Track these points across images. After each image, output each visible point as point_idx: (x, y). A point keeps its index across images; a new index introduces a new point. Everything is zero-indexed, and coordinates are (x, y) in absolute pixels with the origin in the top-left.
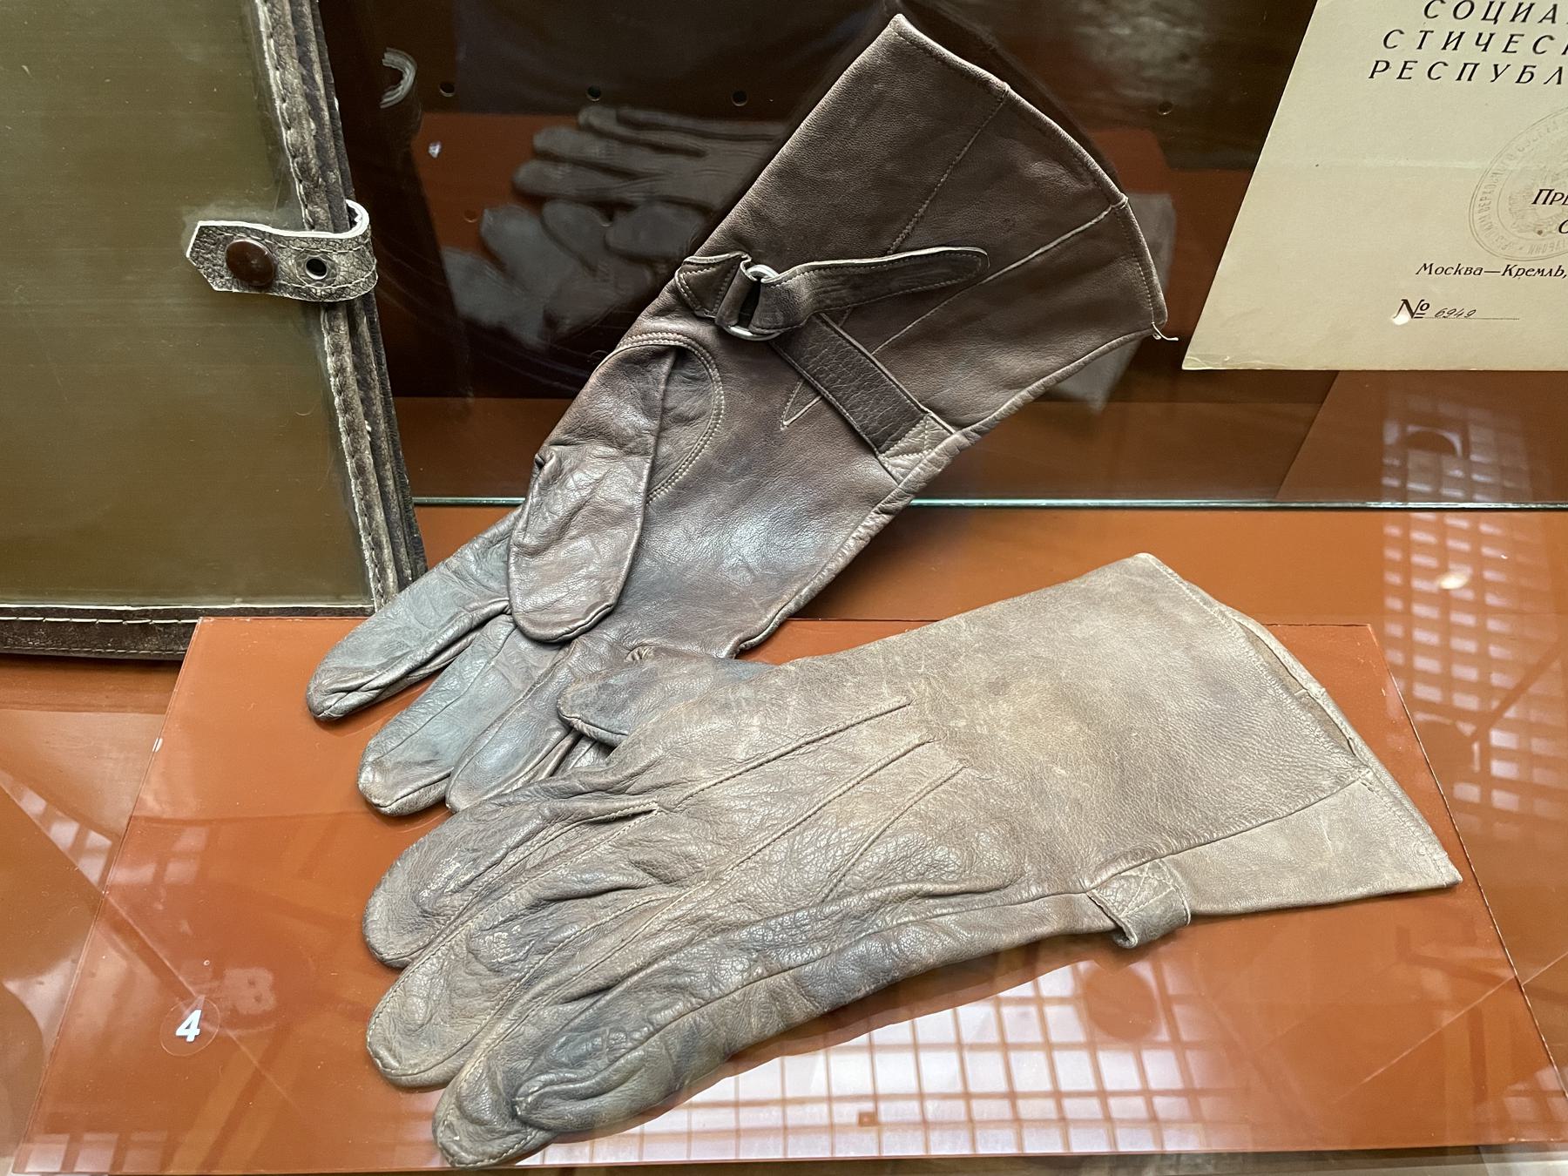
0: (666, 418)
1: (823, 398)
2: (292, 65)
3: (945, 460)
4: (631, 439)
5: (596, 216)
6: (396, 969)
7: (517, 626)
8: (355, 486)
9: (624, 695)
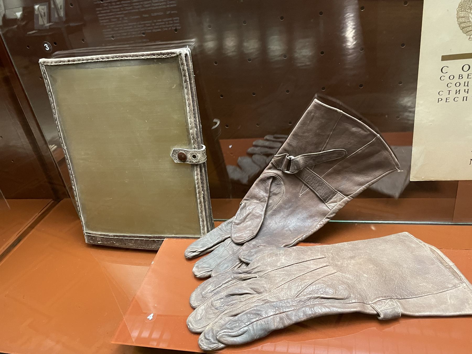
0: (271, 194)
1: (310, 189)
2: (192, 118)
3: (344, 204)
4: (262, 198)
5: (265, 158)
6: (194, 309)
7: (232, 241)
8: (199, 206)
9: (253, 253)
